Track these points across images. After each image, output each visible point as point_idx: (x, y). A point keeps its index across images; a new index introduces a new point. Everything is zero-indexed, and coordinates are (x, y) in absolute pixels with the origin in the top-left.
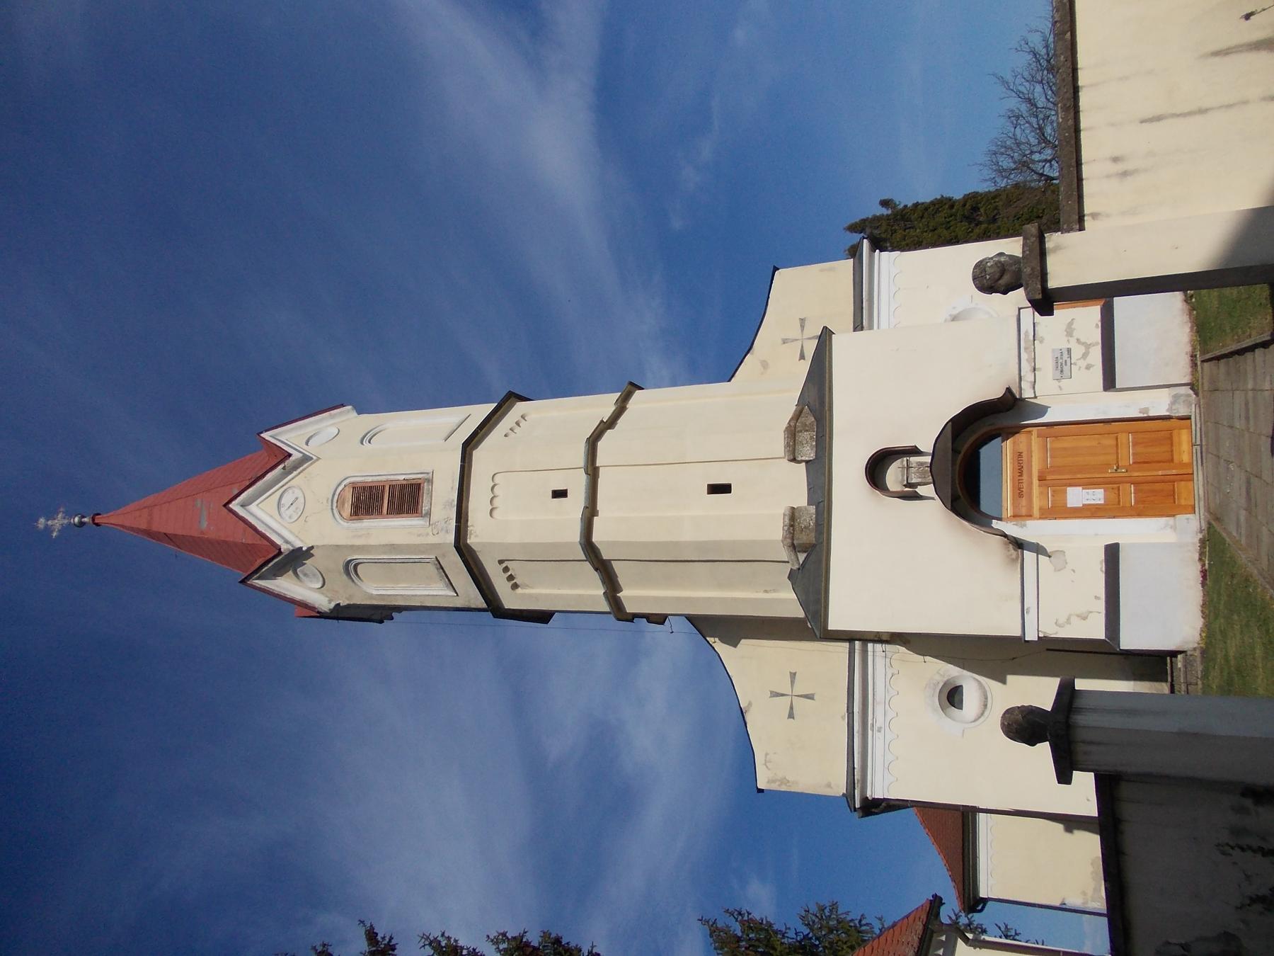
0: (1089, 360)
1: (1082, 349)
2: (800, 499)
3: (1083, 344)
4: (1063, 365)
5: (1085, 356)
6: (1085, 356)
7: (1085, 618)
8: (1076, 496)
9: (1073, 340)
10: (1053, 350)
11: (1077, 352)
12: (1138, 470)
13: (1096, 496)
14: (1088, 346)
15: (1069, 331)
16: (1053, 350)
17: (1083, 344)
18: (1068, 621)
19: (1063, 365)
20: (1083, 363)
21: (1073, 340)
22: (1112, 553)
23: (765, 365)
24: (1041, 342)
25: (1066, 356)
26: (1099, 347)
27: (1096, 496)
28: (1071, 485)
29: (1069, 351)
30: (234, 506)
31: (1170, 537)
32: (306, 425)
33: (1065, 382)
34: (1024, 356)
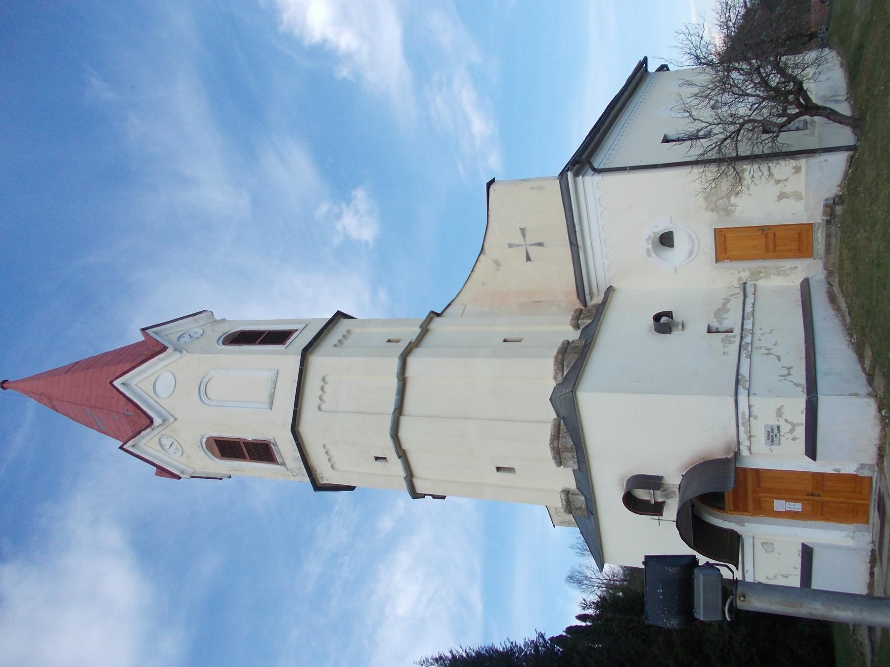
0: (795, 434)
1: (789, 427)
2: (572, 485)
3: (790, 423)
4: (773, 436)
5: (791, 431)
6: (791, 431)
7: (786, 577)
8: (780, 505)
9: (782, 421)
10: (766, 426)
11: (785, 428)
12: (798, 197)
13: (797, 507)
14: (794, 426)
15: (779, 413)
16: (766, 426)
17: (790, 423)
18: (775, 577)
19: (773, 436)
20: (790, 436)
21: (782, 421)
22: (807, 553)
23: (497, 263)
24: (756, 418)
25: (776, 431)
26: (803, 428)
27: (797, 507)
28: (777, 499)
29: (778, 428)
30: (117, 383)
31: (849, 543)
32: (144, 371)
33: (773, 447)
34: (742, 429)
